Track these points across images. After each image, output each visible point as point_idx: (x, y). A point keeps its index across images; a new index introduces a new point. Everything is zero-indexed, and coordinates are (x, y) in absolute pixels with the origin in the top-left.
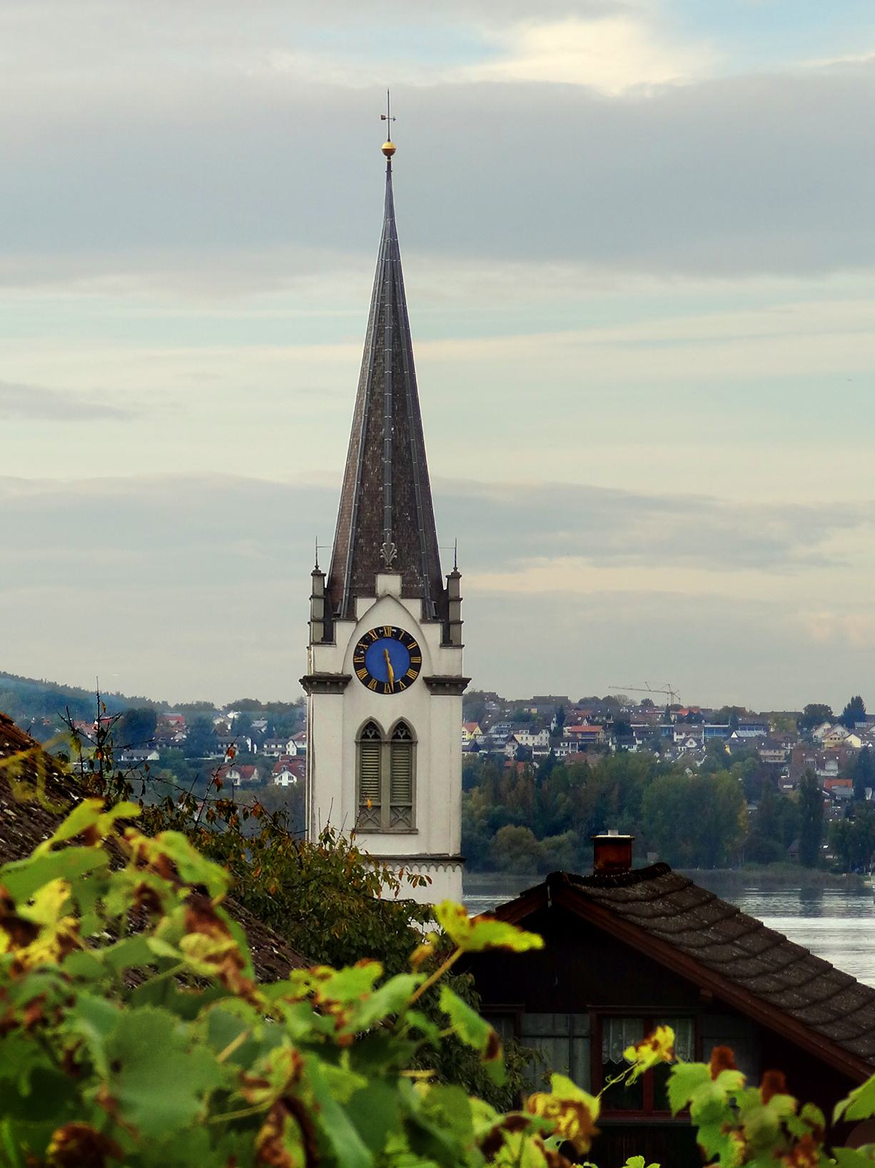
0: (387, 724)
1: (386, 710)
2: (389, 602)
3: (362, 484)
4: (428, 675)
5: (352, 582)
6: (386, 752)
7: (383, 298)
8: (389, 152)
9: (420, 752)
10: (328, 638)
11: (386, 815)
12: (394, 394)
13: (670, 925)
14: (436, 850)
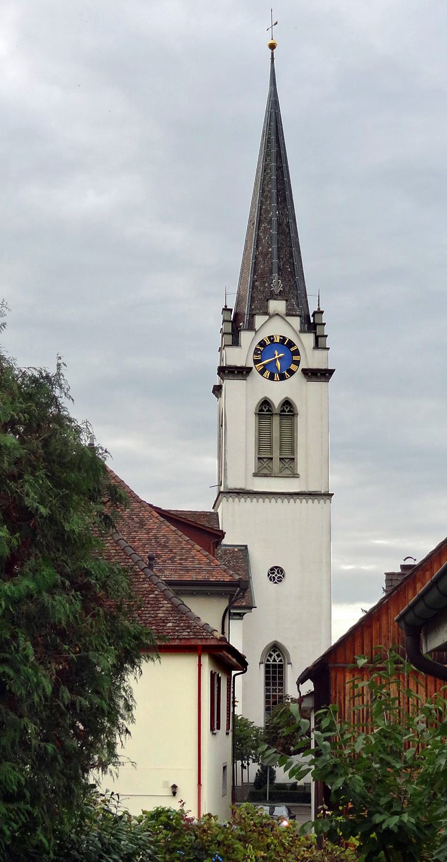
0: (277, 402)
1: (277, 392)
2: (277, 319)
3: (257, 247)
4: (305, 367)
5: (251, 310)
6: (276, 420)
7: (270, 134)
8: (272, 47)
9: (300, 421)
10: (236, 343)
11: (276, 463)
12: (278, 191)
13: (424, 641)
14: (312, 489)
